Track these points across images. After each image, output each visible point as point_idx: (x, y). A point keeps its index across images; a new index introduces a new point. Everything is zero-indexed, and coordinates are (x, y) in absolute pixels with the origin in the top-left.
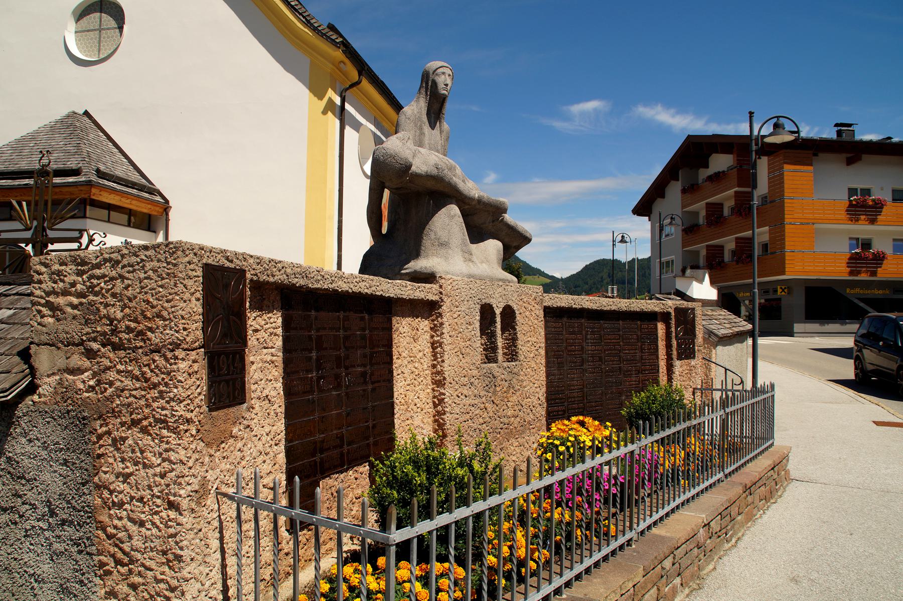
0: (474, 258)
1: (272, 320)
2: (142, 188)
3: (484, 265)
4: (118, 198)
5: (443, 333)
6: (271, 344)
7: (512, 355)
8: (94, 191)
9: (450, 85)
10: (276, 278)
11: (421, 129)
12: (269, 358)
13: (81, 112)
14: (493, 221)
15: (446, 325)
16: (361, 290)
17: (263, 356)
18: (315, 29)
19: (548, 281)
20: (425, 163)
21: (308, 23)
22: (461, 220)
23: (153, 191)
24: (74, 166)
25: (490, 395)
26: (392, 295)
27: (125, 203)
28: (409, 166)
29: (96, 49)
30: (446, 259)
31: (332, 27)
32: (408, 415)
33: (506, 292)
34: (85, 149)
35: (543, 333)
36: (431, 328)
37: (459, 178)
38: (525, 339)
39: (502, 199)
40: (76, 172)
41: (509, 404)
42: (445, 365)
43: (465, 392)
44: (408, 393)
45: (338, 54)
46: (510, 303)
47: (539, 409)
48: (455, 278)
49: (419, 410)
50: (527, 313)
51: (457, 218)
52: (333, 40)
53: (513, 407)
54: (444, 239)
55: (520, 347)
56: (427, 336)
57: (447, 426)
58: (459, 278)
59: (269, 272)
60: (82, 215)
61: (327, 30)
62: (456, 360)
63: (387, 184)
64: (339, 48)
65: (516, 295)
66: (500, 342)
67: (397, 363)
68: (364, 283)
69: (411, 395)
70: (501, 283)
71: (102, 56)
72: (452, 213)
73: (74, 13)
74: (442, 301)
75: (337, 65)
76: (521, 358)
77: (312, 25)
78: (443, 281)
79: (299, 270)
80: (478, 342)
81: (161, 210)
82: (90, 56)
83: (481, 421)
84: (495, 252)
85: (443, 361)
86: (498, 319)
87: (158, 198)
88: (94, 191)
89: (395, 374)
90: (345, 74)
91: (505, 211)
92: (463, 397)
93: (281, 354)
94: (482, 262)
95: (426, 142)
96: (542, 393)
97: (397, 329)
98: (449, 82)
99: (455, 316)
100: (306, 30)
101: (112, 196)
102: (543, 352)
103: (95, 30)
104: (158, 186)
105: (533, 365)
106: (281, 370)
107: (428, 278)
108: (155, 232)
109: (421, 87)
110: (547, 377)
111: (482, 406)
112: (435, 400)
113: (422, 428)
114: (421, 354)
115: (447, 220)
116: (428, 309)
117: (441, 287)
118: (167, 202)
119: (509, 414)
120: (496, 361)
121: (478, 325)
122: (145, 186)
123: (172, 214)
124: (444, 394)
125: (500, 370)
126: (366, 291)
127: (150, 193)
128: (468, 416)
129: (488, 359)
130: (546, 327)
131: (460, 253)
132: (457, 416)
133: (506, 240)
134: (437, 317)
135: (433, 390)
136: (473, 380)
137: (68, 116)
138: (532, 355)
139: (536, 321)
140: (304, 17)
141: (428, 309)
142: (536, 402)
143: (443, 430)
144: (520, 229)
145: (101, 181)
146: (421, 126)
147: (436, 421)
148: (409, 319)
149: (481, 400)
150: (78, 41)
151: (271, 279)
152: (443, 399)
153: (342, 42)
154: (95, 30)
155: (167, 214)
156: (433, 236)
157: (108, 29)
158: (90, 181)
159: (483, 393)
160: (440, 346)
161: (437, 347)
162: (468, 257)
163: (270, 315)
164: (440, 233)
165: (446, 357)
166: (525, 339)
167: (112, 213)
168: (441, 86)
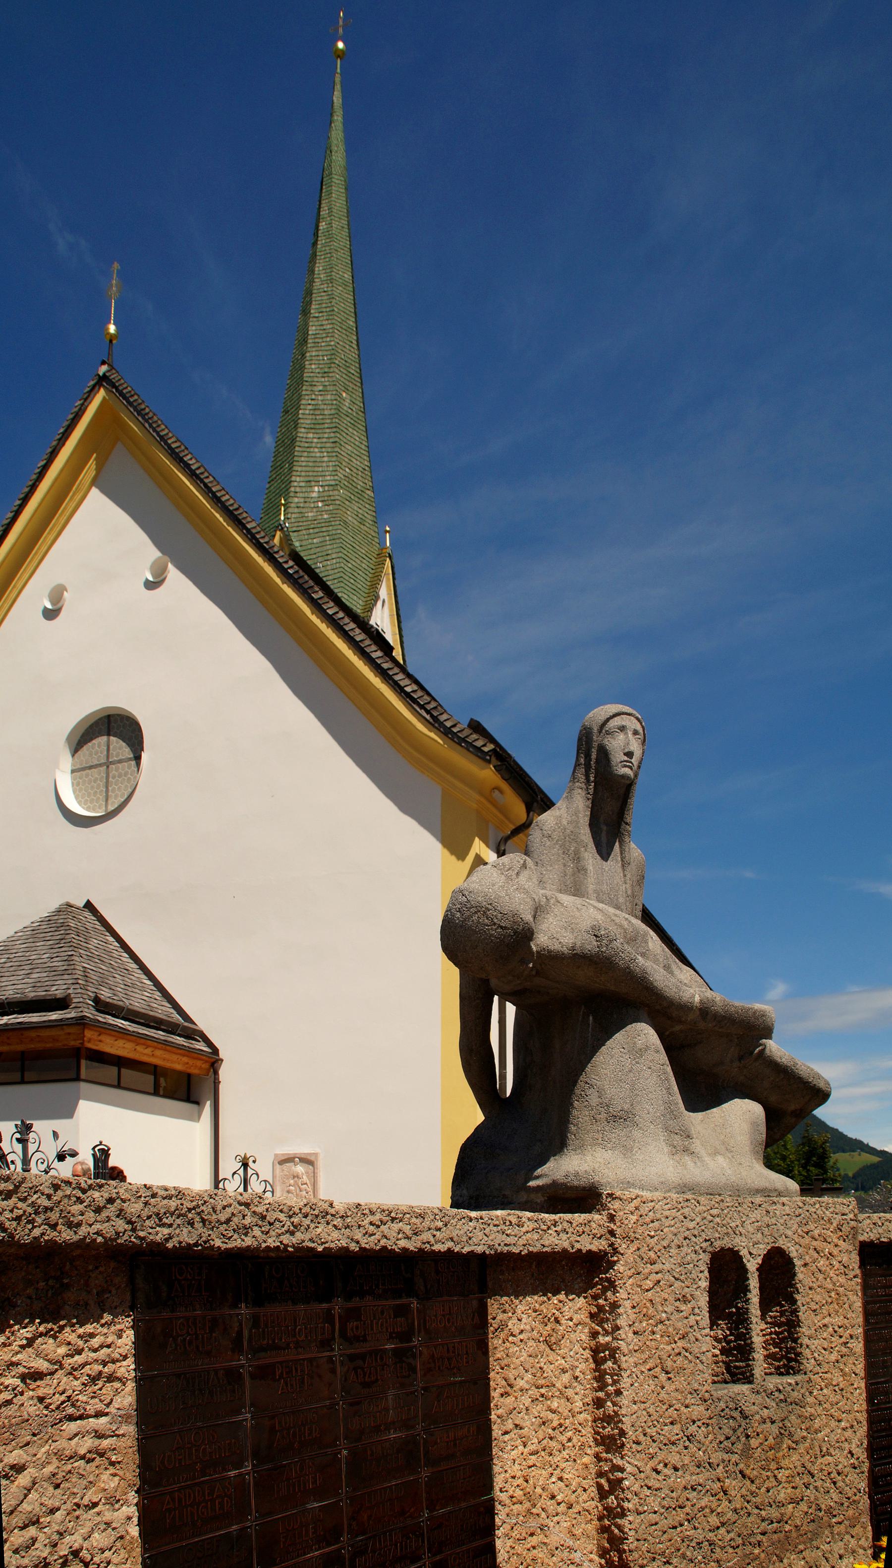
0: (697, 1145)
1: (96, 1342)
2: (172, 1028)
3: (720, 1159)
4: (129, 1045)
5: (617, 1328)
6: (95, 1405)
7: (787, 1360)
8: (88, 1034)
9: (638, 753)
10: (83, 1231)
11: (577, 858)
12: (85, 1445)
13: (81, 903)
14: (741, 1058)
15: (626, 1308)
16: (389, 1244)
17: (62, 1444)
18: (447, 732)
19: (875, 1159)
20: (570, 926)
21: (435, 723)
22: (663, 1057)
23: (193, 1033)
24: (60, 994)
25: (735, 1458)
26: (479, 1249)
27: (143, 1054)
28: (525, 935)
29: (102, 797)
30: (627, 1151)
31: (476, 727)
32: (533, 1524)
33: (775, 1214)
34: (80, 964)
35: (858, 1304)
36: (592, 1316)
37: (656, 961)
38: (818, 1321)
39: (757, 1006)
40: (62, 1003)
41: (782, 1475)
42: (624, 1401)
43: (674, 1459)
44: (534, 1472)
45: (488, 774)
46: (782, 1243)
47: (853, 1477)
48: (647, 1194)
49: (562, 1508)
50: (822, 1262)
51: (650, 1055)
52: (479, 749)
53: (790, 1479)
54: (619, 1105)
55: (805, 1341)
56: (583, 1335)
57: (631, 1543)
58: (657, 1195)
59: (54, 1216)
60: (74, 1076)
61: (467, 732)
62: (650, 1386)
63: (494, 982)
64: (489, 762)
65: (794, 1223)
66: (759, 1331)
67: (500, 1405)
68: (396, 1226)
69: (540, 1476)
70: (758, 1199)
71: (111, 808)
72: (640, 1043)
73: (69, 739)
74: (615, 1251)
75: (489, 795)
76: (809, 1365)
77: (441, 724)
78: (616, 1205)
79: (173, 1204)
80: (707, 1344)
81: (206, 1066)
82: (94, 810)
83: (714, 1520)
84: (746, 1127)
85: (618, 1393)
86: (754, 1283)
87: (201, 1046)
88: (88, 1034)
89: (496, 1432)
90: (504, 811)
91: (767, 1032)
92: (668, 1471)
93: (130, 1429)
94: (716, 1153)
95: (591, 888)
96: (857, 1440)
97: (503, 1326)
98: (635, 746)
99: (649, 1284)
100: (432, 735)
101: (120, 1043)
102: (858, 1346)
103: (100, 765)
104: (202, 1024)
105: (837, 1378)
106: (131, 1472)
107: (583, 1198)
108: (197, 1103)
109: (577, 764)
110: (870, 1400)
111: (717, 1486)
112: (603, 1481)
113: (571, 1549)
114: (566, 1378)
115: (627, 1061)
116: (584, 1272)
117: (612, 1218)
118: (215, 1051)
119: (782, 1496)
120: (749, 1380)
121: (703, 1300)
122: (177, 1025)
123: (224, 1072)
124: (622, 1470)
125: (759, 1399)
126: (403, 1243)
127: (188, 1037)
128: (681, 1515)
129: (732, 1375)
130: (865, 1287)
131: (662, 1136)
132: (654, 1518)
133: (773, 1098)
134: (605, 1290)
135: (597, 1456)
136: (693, 1428)
137: (59, 911)
138: (833, 1357)
139: (842, 1279)
140: (428, 712)
141: (584, 1272)
142: (845, 1462)
143: (621, 1552)
144: (803, 1072)
145: (101, 1018)
146: (577, 852)
147: (604, 1530)
148: (533, 1300)
149: (713, 1474)
150: (75, 785)
151: (66, 1235)
152: (621, 1480)
153: (494, 750)
154: (100, 765)
155: (216, 1073)
156: (594, 1100)
157: (120, 761)
158: (83, 1018)
159: (717, 1457)
160: (612, 1356)
161: (604, 1360)
162: (682, 1143)
163: (89, 1328)
164: (611, 1091)
165: (625, 1382)
166: (818, 1321)
167: (123, 1070)
168: (618, 757)
